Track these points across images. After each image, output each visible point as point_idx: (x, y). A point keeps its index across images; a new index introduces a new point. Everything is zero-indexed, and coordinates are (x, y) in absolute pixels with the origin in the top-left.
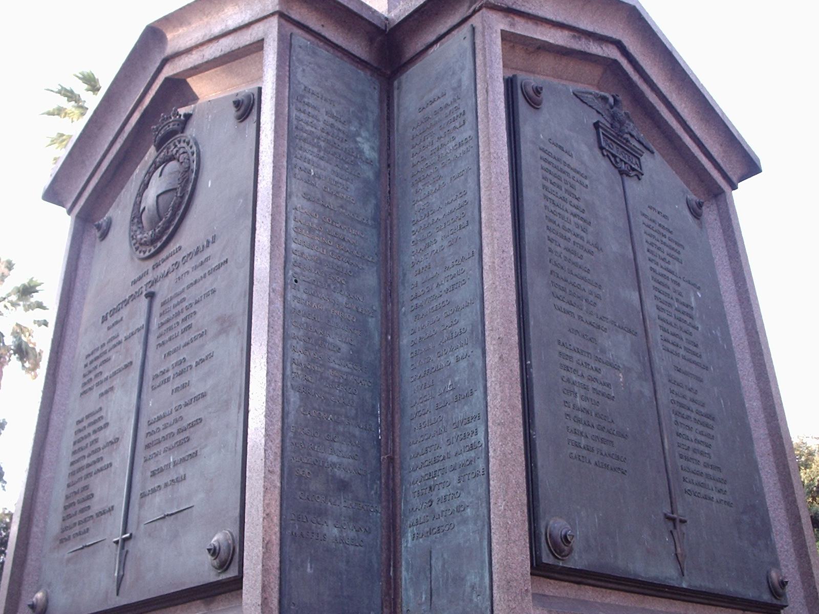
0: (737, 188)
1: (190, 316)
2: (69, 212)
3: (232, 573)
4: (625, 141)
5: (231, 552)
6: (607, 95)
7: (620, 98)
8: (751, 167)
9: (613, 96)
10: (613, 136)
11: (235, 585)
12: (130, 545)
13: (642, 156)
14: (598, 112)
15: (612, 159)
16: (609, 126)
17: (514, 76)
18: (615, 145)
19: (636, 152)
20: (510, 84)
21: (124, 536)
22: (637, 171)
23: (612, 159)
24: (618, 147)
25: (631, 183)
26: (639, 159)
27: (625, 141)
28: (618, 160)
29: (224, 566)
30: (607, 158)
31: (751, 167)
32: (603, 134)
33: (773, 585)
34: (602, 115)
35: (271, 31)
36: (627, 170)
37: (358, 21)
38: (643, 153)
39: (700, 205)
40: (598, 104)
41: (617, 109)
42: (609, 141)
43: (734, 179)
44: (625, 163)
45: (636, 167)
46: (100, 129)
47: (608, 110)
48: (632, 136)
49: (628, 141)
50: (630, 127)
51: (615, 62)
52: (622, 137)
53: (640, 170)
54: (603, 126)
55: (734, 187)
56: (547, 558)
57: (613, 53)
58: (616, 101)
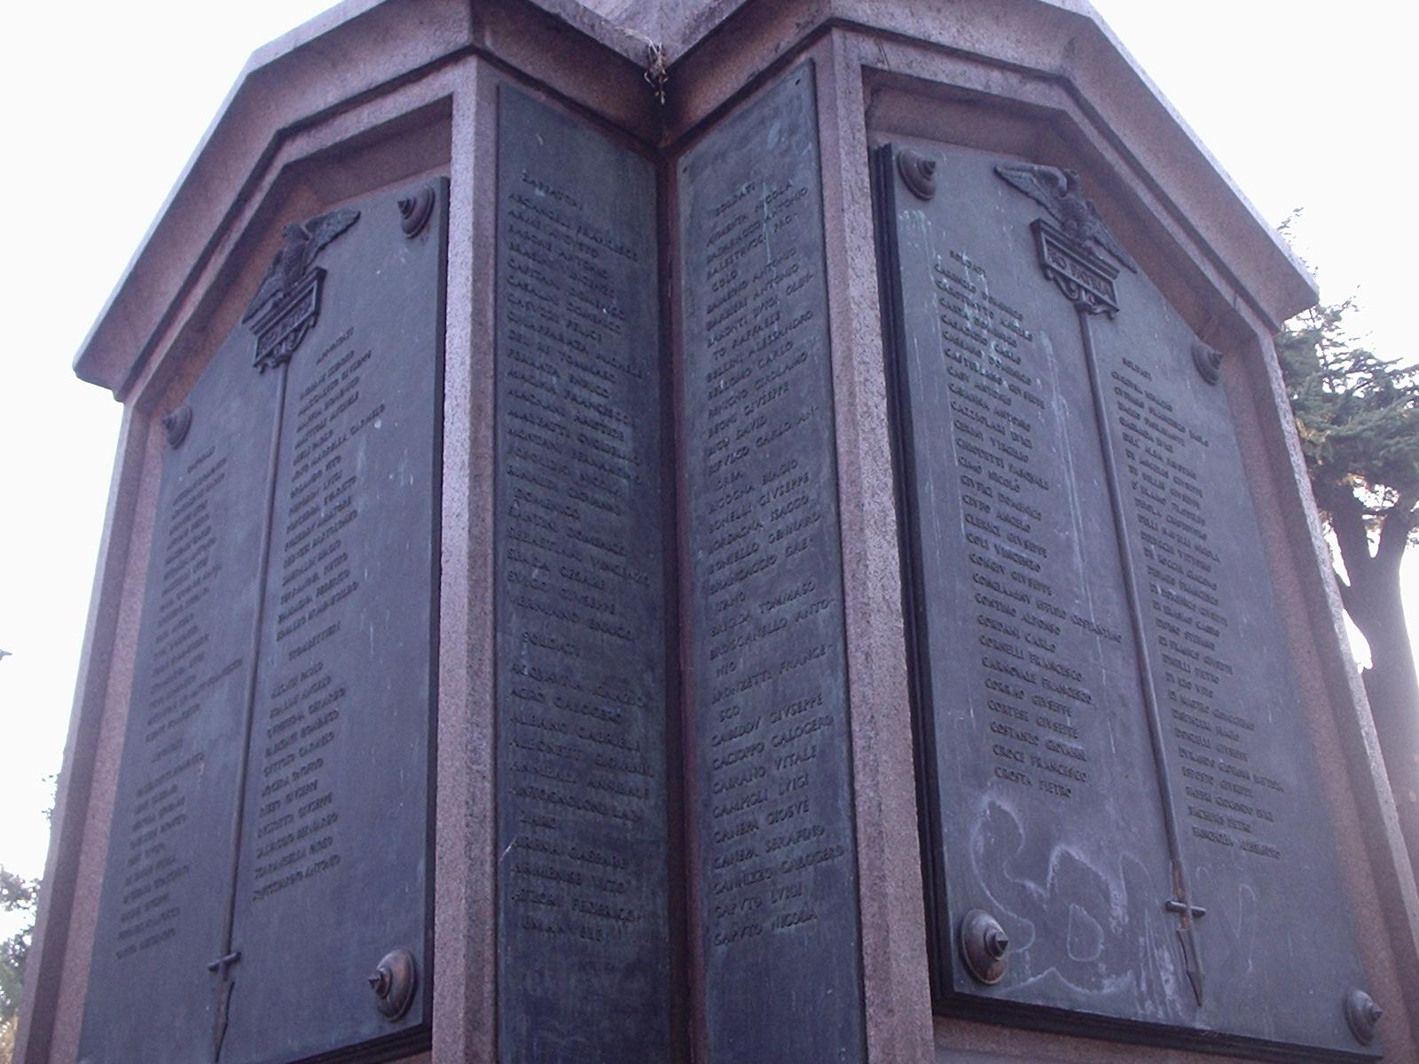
2: (122, 396)
3: (414, 1019)
5: (412, 985)
6: (1058, 173)
7: (1077, 177)
9: (1066, 174)
10: (1065, 244)
11: (421, 1039)
12: (236, 972)
13: (1115, 278)
14: (1039, 203)
15: (1062, 284)
16: (1057, 226)
17: (888, 147)
18: (1068, 262)
20: (880, 160)
21: (228, 958)
22: (1106, 304)
23: (1065, 286)
24: (1075, 264)
25: (1097, 328)
27: (1085, 253)
28: (1073, 287)
29: (397, 1011)
32: (1047, 242)
34: (1047, 208)
35: (463, 82)
36: (1089, 306)
37: (578, 44)
38: (1118, 272)
39: (1216, 361)
40: (1043, 194)
42: (1059, 255)
43: (1272, 315)
44: (1087, 291)
45: (1106, 298)
46: (67, 815)
47: (1056, 198)
48: (1097, 242)
49: (1091, 252)
50: (1094, 227)
51: (1060, 114)
52: (1080, 245)
53: (1111, 303)
54: (1047, 229)
56: (963, 985)
57: (1054, 99)
58: (1071, 182)
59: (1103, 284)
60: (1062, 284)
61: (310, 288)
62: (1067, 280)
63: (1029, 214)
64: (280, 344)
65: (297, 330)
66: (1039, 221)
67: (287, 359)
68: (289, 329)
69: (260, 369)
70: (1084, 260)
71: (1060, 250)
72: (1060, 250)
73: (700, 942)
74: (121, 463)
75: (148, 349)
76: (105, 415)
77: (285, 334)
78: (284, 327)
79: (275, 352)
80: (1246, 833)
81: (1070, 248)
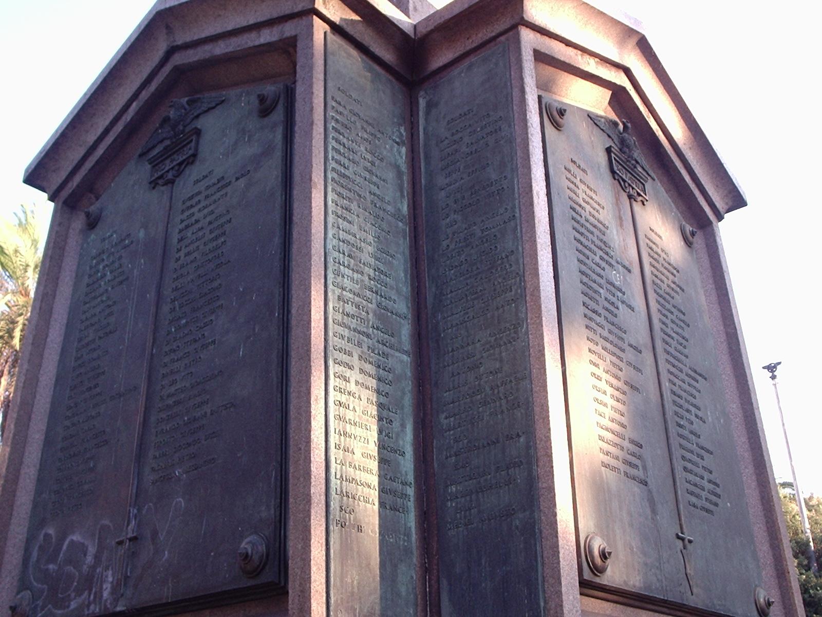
0: (723, 218)
1: (611, 265)
2: (51, 199)
4: (632, 167)
8: (737, 201)
15: (622, 183)
19: (641, 178)
26: (644, 185)
30: (616, 181)
31: (737, 201)
33: (760, 605)
34: (613, 140)
39: (693, 234)
41: (627, 135)
42: (620, 167)
51: (624, 89)
55: (720, 218)
57: (621, 80)
59: (641, 185)
60: (622, 183)
61: (190, 139)
62: (624, 181)
63: (609, 143)
64: (168, 171)
65: (180, 164)
66: (611, 146)
67: (172, 182)
68: (175, 163)
69: (153, 185)
70: (632, 171)
71: (620, 164)
72: (620, 164)
73: (419, 602)
74: (108, 70)
75: (72, 172)
76: (41, 208)
77: (172, 166)
78: (172, 161)
79: (165, 176)
80: (344, 109)
81: (632, 169)
